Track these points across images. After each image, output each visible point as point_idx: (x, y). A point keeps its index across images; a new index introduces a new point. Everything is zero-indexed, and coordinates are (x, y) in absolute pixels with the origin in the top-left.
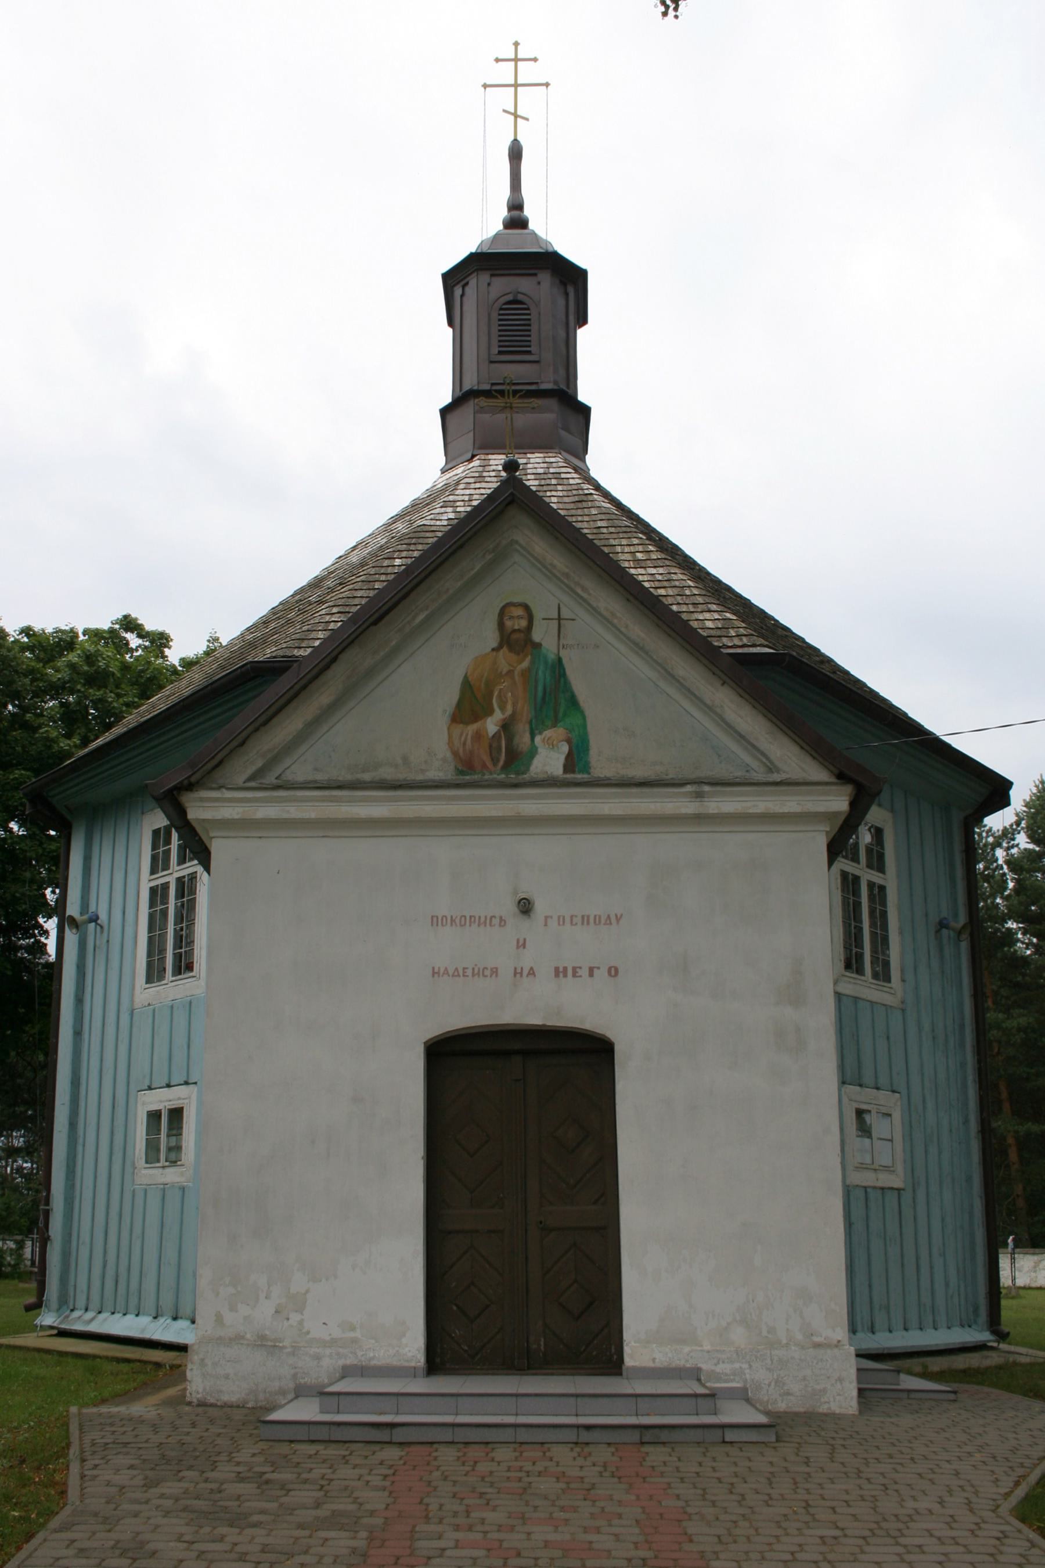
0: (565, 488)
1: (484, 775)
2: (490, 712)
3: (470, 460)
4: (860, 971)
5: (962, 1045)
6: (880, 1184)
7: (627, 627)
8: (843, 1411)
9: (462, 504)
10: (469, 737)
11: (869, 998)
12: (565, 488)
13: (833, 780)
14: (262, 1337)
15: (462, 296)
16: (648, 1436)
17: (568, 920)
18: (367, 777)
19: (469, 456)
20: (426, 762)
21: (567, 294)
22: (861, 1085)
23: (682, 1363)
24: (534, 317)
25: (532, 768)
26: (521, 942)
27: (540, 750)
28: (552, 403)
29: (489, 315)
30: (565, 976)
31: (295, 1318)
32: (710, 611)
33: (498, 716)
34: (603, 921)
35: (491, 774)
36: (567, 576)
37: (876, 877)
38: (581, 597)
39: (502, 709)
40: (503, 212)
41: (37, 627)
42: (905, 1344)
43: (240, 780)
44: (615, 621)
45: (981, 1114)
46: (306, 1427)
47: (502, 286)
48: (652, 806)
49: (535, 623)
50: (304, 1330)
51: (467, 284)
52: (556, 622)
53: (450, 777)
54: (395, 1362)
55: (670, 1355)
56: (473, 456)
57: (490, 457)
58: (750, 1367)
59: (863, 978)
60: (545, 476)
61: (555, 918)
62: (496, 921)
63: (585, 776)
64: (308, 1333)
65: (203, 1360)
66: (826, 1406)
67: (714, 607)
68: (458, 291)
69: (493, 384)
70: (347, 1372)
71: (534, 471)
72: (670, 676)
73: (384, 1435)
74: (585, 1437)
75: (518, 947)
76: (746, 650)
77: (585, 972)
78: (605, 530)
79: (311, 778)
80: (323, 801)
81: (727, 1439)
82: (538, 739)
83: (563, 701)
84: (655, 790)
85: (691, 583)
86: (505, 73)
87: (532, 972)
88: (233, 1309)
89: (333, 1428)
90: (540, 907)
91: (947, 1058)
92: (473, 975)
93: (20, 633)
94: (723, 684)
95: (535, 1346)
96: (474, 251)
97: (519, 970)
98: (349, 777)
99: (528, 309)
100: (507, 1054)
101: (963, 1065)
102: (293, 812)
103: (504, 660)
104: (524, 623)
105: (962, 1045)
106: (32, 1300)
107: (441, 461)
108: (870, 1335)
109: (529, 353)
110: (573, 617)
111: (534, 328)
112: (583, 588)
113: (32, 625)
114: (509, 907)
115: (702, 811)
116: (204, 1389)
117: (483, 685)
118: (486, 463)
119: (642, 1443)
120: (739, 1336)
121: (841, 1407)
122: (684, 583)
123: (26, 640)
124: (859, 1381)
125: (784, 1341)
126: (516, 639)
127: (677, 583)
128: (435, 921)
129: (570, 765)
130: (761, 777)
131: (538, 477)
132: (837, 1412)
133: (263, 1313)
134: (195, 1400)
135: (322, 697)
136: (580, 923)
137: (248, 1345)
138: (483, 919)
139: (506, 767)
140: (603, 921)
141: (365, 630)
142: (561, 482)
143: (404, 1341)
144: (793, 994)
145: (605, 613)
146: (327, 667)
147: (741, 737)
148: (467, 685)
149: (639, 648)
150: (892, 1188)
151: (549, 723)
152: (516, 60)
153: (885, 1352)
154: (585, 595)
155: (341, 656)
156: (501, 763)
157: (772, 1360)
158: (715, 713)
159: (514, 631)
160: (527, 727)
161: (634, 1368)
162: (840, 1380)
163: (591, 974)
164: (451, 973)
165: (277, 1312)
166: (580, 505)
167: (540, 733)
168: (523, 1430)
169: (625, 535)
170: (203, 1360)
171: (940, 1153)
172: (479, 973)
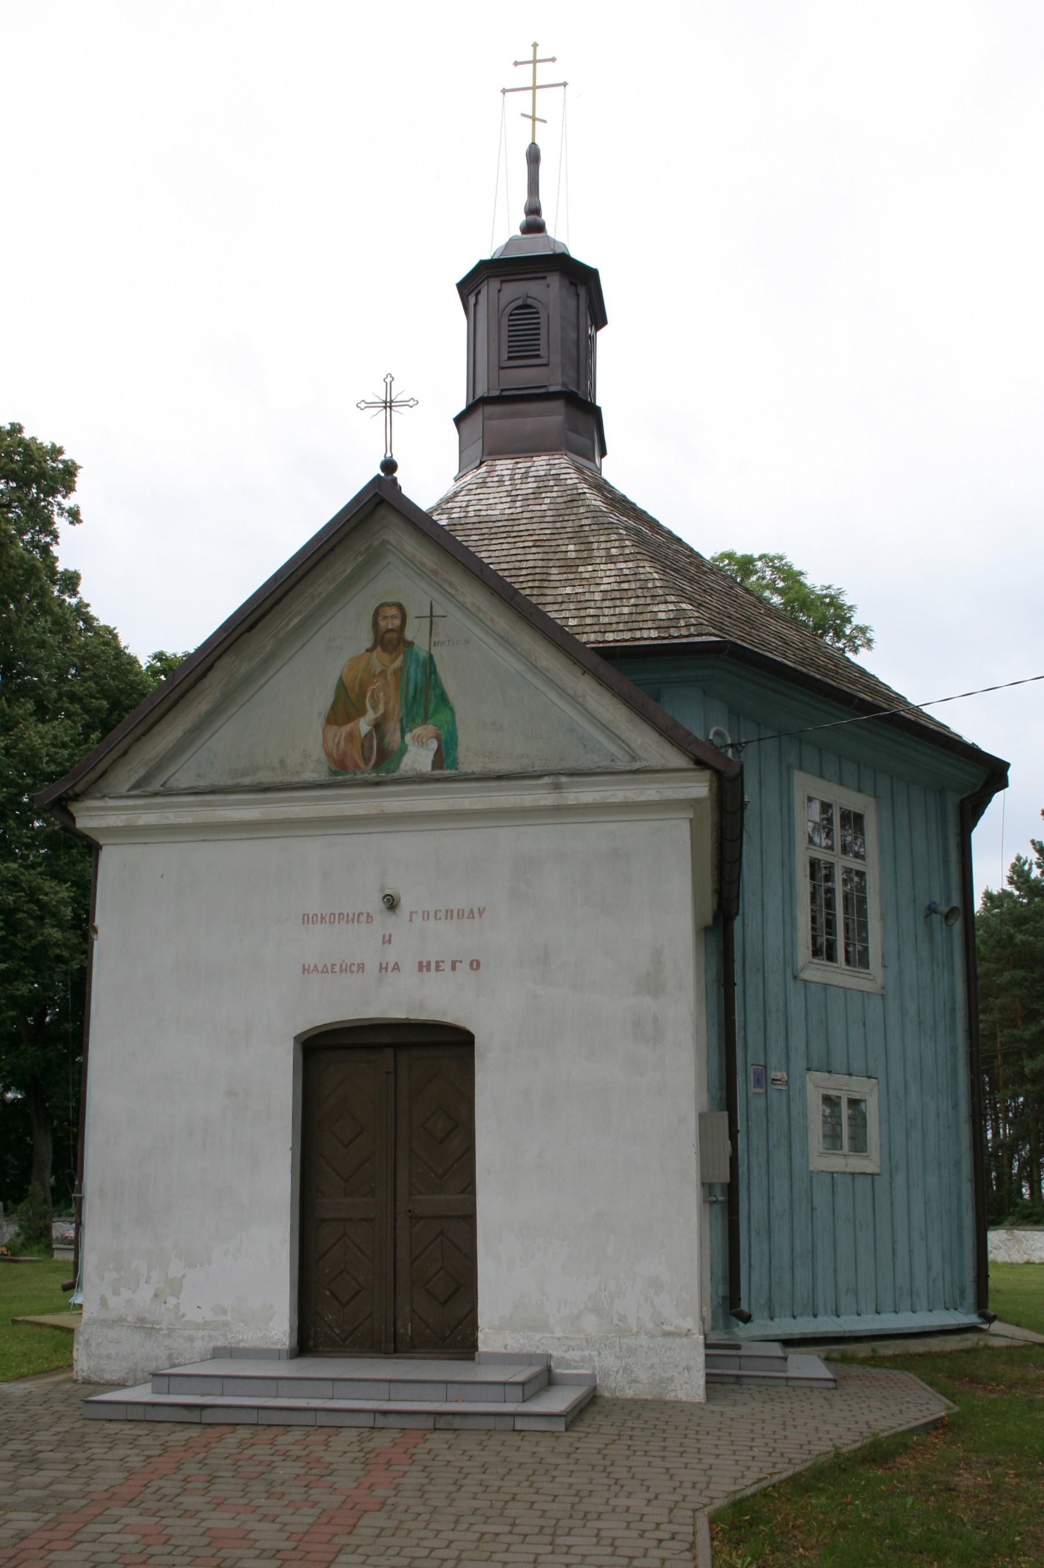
0: (561, 488)
1: (356, 774)
2: (363, 712)
3: (478, 467)
4: (831, 957)
5: (953, 1029)
6: (849, 1169)
7: (492, 621)
8: (689, 1399)
9: (458, 510)
10: (343, 738)
11: (842, 985)
12: (561, 488)
13: (692, 766)
14: (142, 1320)
15: (475, 304)
16: (442, 1423)
17: (432, 915)
18: (246, 781)
19: (478, 462)
20: (301, 764)
21: (578, 295)
22: (829, 1072)
23: (533, 1350)
24: (543, 321)
25: (402, 766)
26: (387, 938)
27: (409, 748)
28: (559, 405)
29: (499, 321)
30: (429, 970)
31: (172, 1301)
32: (666, 602)
33: (371, 715)
34: (466, 915)
35: (362, 773)
36: (435, 573)
37: (856, 865)
38: (451, 594)
39: (375, 708)
40: (521, 218)
41: (169, 652)
42: (869, 1327)
43: (124, 789)
44: (481, 616)
45: (972, 1097)
46: (123, 1407)
47: (513, 291)
48: (512, 799)
49: (408, 621)
50: (180, 1314)
51: (479, 292)
52: (428, 619)
53: (323, 778)
54: (262, 1345)
55: (522, 1341)
56: (482, 463)
57: (497, 462)
58: (600, 1354)
59: (834, 964)
60: (545, 478)
61: (420, 914)
62: (363, 918)
63: (453, 772)
64: (184, 1316)
65: (87, 1341)
66: (673, 1394)
67: (672, 598)
68: (472, 300)
69: (502, 390)
70: (218, 1353)
71: (535, 474)
72: (535, 668)
73: (194, 1416)
74: (381, 1421)
75: (384, 943)
77: (447, 966)
78: (587, 528)
79: (193, 784)
80: (199, 806)
81: (517, 1427)
83: (433, 698)
84: (513, 783)
85: (656, 576)
86: (523, 76)
87: (396, 967)
88: (116, 1293)
89: (148, 1408)
90: (406, 904)
91: (935, 1042)
92: (341, 971)
93: (154, 659)
94: (583, 674)
95: (402, 1331)
96: (487, 256)
97: (384, 966)
98: (230, 782)
99: (537, 313)
100: (380, 1047)
101: (953, 1050)
102: (172, 817)
104: (397, 622)
105: (953, 1029)
106: (70, 1281)
107: (455, 470)
108: (835, 1318)
109: (538, 356)
110: (444, 614)
111: (543, 332)
112: (451, 585)
113: (164, 650)
114: (375, 904)
115: (560, 802)
116: (89, 1368)
117: (357, 687)
118: (492, 468)
119: (436, 1429)
120: (590, 1324)
121: (687, 1395)
122: (649, 576)
123: (159, 664)
124: (707, 1367)
125: (635, 1330)
126: (389, 639)
127: (642, 577)
128: (306, 919)
129: (439, 761)
130: (620, 766)
131: (538, 479)
132: (684, 1400)
133: (143, 1297)
134: (80, 1378)
135: (201, 704)
136: (443, 917)
137: (128, 1327)
138: (351, 916)
139: (377, 766)
140: (466, 915)
141: (238, 638)
142: (558, 483)
143: (271, 1324)
144: (652, 984)
145: (471, 609)
146: (203, 675)
147: (604, 727)
148: (342, 688)
149: (504, 641)
150: (864, 1174)
151: (419, 720)
152: (535, 62)
153: (847, 1335)
154: (452, 592)
155: (216, 665)
157: (621, 1348)
158: (578, 703)
159: (389, 631)
160: (398, 726)
161: (487, 1353)
162: (688, 1368)
163: (454, 968)
164: (320, 969)
165: (155, 1296)
166: (570, 505)
167: (411, 731)
168: (323, 1413)
169: (606, 532)
170: (87, 1341)
171: (924, 1137)
172: (346, 969)
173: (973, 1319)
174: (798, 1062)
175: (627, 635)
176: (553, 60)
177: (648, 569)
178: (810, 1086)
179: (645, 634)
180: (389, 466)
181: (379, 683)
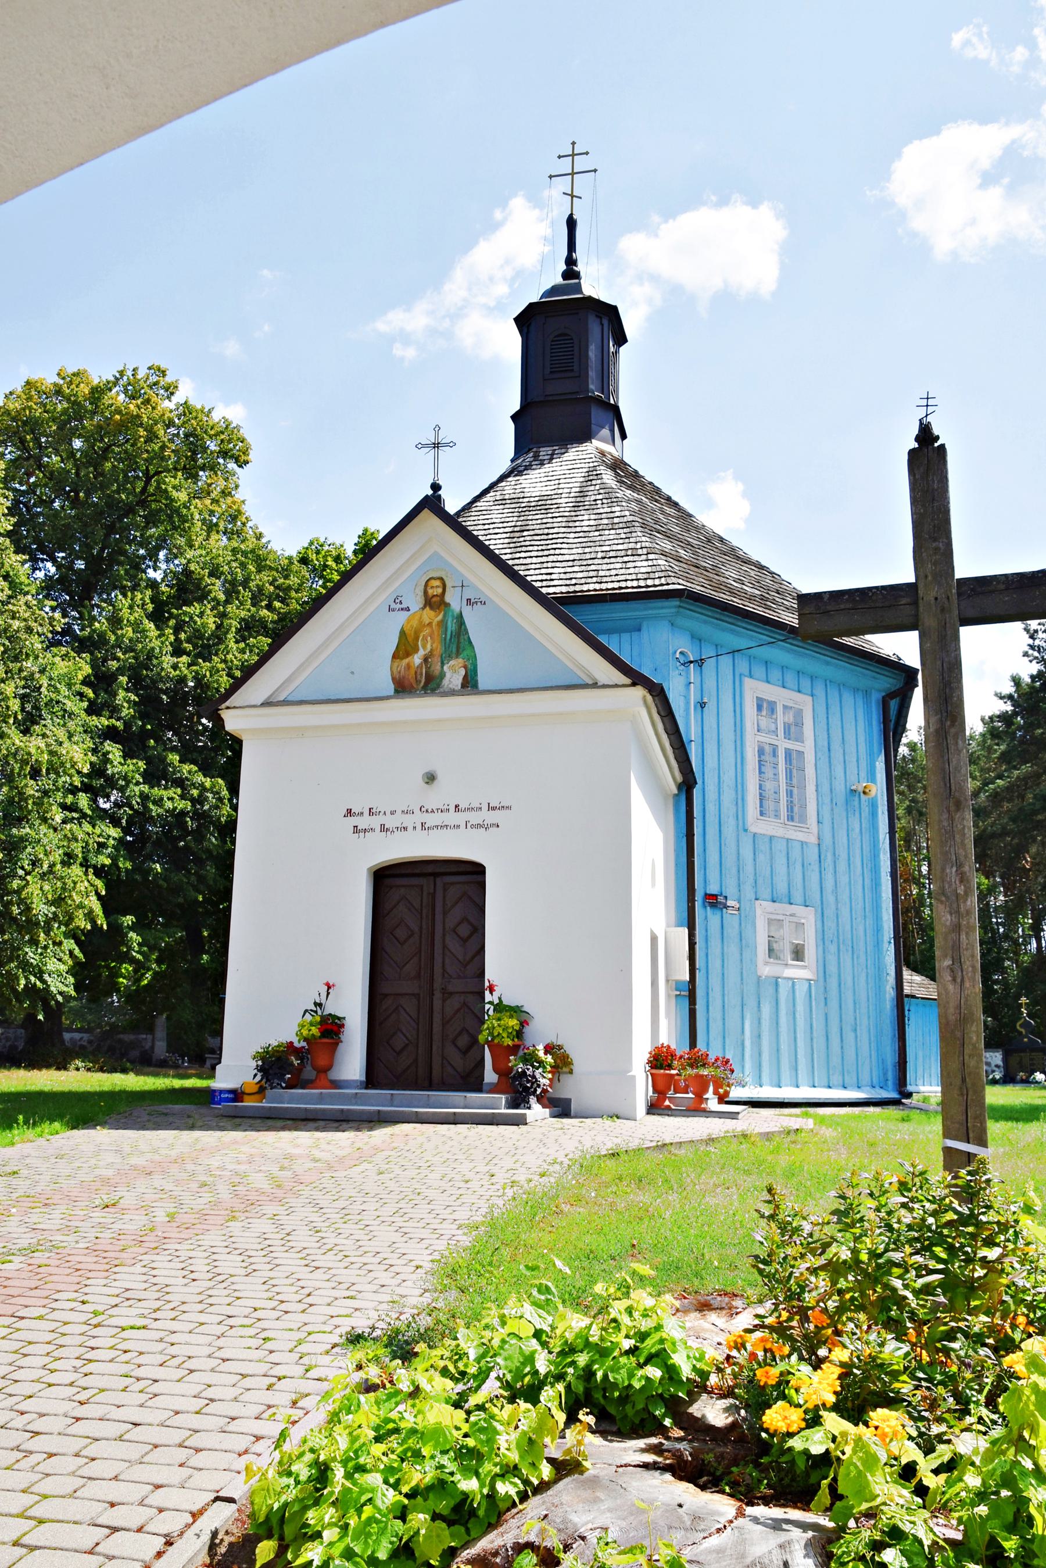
2: (417, 650)
21: (602, 325)
33: (422, 652)
39: (424, 648)
76: (666, 588)
82: (445, 668)
86: (565, 166)
103: (428, 615)
104: (440, 590)
107: (512, 455)
109: (572, 370)
122: (638, 539)
148: (403, 633)
151: (454, 655)
152: (573, 155)
156: (422, 684)
159: (434, 596)
173: (894, 1095)
174: (748, 893)
175: (616, 585)
176: (587, 153)
177: (640, 534)
178: (759, 912)
179: (629, 584)
180: (436, 487)
181: (427, 631)
